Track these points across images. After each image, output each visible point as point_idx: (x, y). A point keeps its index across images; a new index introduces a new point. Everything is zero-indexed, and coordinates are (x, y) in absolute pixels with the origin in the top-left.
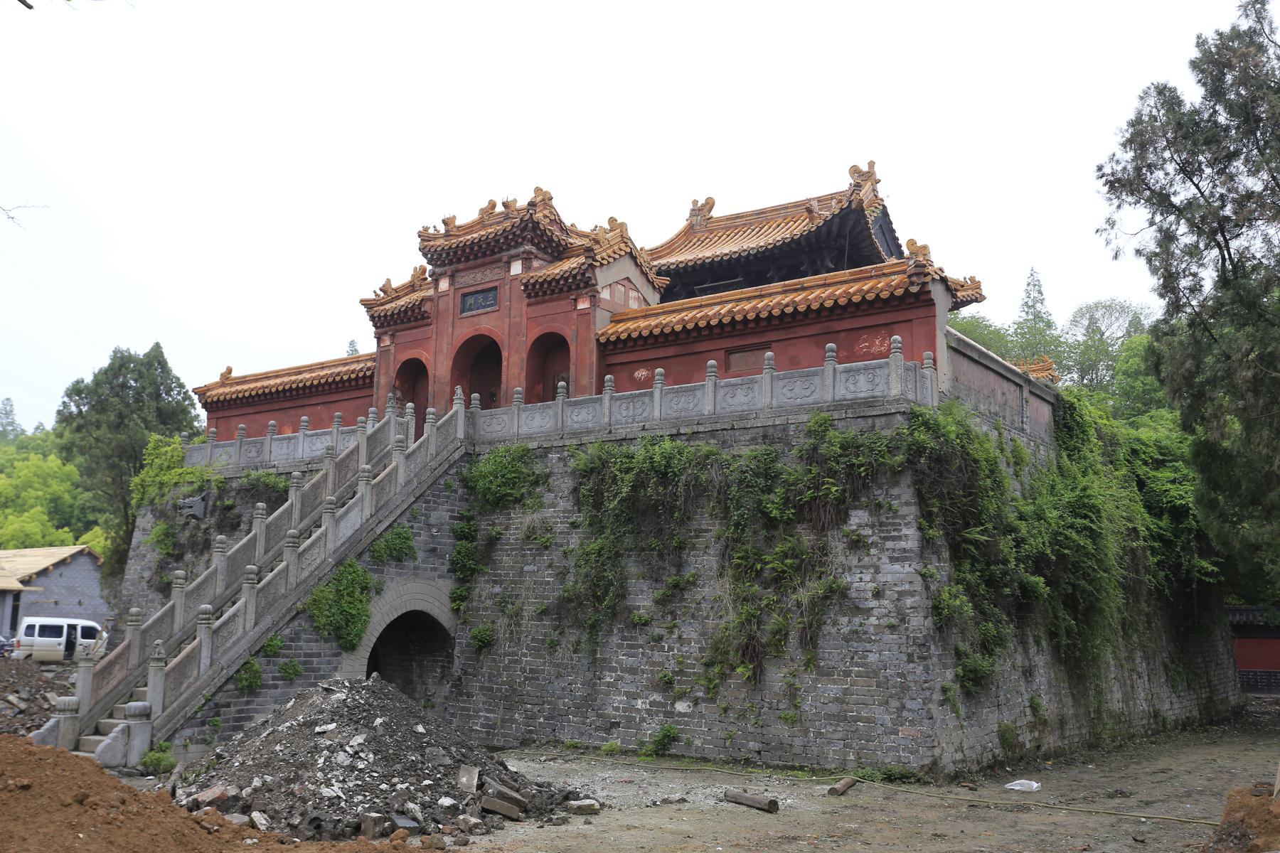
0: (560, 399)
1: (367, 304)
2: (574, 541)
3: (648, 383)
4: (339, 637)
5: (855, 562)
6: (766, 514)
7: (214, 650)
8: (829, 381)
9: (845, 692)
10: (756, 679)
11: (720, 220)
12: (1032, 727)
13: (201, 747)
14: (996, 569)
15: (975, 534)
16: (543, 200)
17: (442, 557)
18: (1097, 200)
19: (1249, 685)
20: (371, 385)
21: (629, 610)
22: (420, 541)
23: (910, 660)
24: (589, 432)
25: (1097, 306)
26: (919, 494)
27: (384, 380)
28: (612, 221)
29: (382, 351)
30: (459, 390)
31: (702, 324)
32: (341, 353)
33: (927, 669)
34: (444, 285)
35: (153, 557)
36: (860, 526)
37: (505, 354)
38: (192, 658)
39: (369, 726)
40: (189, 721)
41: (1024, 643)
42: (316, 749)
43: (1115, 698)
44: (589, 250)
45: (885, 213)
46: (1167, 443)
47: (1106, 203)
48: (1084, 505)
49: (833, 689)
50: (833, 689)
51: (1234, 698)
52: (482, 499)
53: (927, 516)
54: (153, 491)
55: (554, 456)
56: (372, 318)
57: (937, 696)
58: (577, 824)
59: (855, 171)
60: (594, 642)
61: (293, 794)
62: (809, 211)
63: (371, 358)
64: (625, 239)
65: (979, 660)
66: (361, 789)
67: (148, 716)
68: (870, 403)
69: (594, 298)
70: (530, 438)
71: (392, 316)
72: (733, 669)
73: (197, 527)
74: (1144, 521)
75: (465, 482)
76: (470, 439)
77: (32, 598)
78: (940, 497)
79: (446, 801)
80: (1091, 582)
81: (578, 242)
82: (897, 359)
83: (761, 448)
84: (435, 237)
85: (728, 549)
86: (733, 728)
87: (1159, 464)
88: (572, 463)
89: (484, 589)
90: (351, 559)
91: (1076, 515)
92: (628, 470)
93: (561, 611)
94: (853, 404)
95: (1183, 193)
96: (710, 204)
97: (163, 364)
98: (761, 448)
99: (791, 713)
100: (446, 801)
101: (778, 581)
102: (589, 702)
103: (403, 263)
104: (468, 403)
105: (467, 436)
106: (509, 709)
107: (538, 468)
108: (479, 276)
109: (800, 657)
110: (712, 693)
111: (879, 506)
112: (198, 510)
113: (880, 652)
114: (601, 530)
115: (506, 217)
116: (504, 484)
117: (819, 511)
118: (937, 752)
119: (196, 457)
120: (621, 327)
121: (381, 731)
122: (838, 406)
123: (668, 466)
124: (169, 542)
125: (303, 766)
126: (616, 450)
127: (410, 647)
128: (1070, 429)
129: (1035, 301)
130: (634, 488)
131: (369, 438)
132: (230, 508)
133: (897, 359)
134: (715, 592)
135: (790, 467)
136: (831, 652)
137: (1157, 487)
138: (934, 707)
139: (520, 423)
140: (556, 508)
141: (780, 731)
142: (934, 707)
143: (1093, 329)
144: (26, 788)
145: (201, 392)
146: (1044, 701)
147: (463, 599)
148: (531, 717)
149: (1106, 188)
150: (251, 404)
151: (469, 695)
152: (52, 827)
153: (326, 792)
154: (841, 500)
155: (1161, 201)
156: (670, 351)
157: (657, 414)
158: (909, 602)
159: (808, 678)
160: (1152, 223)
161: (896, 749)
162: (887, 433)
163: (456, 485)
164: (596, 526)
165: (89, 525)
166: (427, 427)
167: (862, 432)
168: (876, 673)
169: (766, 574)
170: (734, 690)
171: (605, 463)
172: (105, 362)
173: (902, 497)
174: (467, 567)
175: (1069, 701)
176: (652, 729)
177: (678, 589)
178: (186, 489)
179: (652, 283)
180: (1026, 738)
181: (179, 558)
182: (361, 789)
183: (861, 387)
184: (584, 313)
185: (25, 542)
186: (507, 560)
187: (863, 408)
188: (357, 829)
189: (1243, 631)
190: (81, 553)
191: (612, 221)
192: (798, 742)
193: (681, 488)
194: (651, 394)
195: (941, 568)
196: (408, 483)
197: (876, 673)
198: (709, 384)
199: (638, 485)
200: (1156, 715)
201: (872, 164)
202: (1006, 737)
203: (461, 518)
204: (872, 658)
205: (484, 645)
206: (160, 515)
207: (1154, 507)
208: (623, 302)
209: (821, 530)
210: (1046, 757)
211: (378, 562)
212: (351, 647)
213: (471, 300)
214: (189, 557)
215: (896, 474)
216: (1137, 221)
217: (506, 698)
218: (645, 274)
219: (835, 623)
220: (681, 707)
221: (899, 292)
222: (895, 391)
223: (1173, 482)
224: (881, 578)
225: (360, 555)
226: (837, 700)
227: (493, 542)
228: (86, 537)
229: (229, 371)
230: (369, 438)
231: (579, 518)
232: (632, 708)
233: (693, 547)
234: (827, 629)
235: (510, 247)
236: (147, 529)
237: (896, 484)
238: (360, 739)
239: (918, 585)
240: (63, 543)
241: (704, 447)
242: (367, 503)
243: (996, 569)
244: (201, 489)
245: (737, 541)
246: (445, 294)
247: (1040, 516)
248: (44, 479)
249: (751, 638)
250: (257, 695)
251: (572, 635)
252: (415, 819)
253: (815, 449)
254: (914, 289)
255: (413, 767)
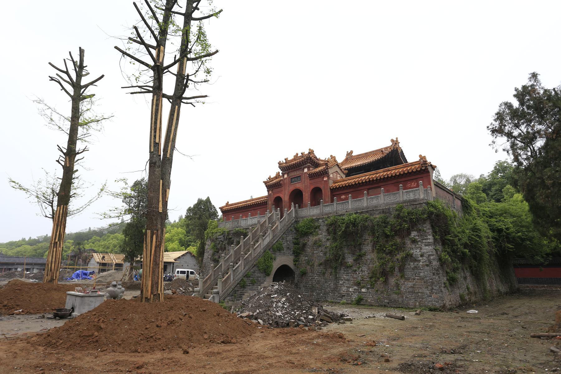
0: (321, 205)
1: (265, 183)
2: (328, 244)
3: (346, 199)
4: (265, 272)
5: (414, 246)
6: (386, 234)
7: (234, 276)
8: (401, 195)
9: (414, 285)
10: (386, 282)
11: (355, 156)
12: (468, 294)
13: (232, 302)
14: (455, 247)
15: (448, 237)
16: (311, 152)
17: (291, 249)
18: (490, 137)
19: (520, 282)
20: (267, 204)
21: (346, 263)
22: (285, 245)
23: (434, 274)
24: (331, 213)
25: (457, 176)
26: (432, 226)
27: (270, 202)
28: (331, 156)
29: (269, 195)
30: (293, 204)
31: (360, 182)
32: (249, 198)
33: (439, 277)
34: (286, 176)
35: (211, 252)
36: (414, 236)
37: (304, 194)
38: (229, 278)
39: (286, 295)
40: (229, 295)
41: (463, 269)
42: (272, 302)
43: (488, 287)
44: (327, 164)
45: (402, 152)
46: (493, 211)
47: (491, 136)
48: (476, 229)
49: (410, 284)
50: (410, 284)
51: (517, 286)
52: (301, 233)
53: (435, 232)
54: (210, 235)
55: (321, 221)
56: (266, 186)
57: (443, 285)
58: (348, 324)
59: (392, 141)
60: (336, 272)
61: (268, 314)
62: (382, 151)
63: (266, 197)
64: (335, 161)
65: (452, 274)
66: (287, 313)
67: (218, 293)
68: (415, 200)
69: (328, 177)
70: (313, 216)
71: (271, 185)
72: (379, 279)
73: (222, 244)
74: (491, 234)
75: (295, 229)
76: (296, 217)
77: (177, 264)
78: (439, 226)
79: (311, 317)
80: (480, 251)
81: (322, 162)
82: (421, 187)
83: (382, 215)
84: (282, 164)
85: (374, 244)
86: (380, 296)
87: (491, 217)
88: (326, 222)
89: (303, 258)
90: (267, 250)
91: (474, 232)
92: (343, 223)
93: (326, 264)
94: (410, 201)
95: (516, 133)
96: (352, 152)
97: (210, 202)
98: (382, 215)
99: (397, 291)
100: (311, 317)
101: (391, 253)
102: (336, 289)
103: (274, 171)
104: (295, 207)
105: (295, 216)
106: (312, 292)
107: (316, 224)
108: (295, 173)
109: (399, 275)
110: (372, 286)
111: (420, 230)
112: (222, 239)
113: (424, 273)
114: (336, 241)
115: (302, 157)
116: (307, 229)
117: (402, 232)
118: (445, 302)
119: (221, 225)
120: (337, 184)
121: (289, 297)
122: (405, 202)
123: (355, 221)
124: (215, 248)
125: (269, 306)
126: (339, 218)
127: (284, 273)
128: (467, 207)
129: (438, 175)
130: (346, 228)
131: (269, 218)
132: (231, 238)
133: (421, 187)
134: (371, 257)
135: (392, 220)
136: (408, 273)
137: (492, 223)
138: (442, 288)
139: (310, 212)
140: (322, 235)
141: (395, 296)
142: (442, 288)
143: (455, 182)
144: (205, 311)
145: (221, 208)
146: (470, 286)
147: (297, 261)
148: (318, 294)
149: (491, 133)
150: (233, 211)
151: (300, 288)
152: (212, 322)
153: (277, 314)
154: (408, 229)
155: (509, 135)
156: (351, 190)
157: (350, 207)
158: (432, 257)
159: (402, 281)
160: (508, 141)
161: (432, 301)
162: (421, 209)
163: (293, 230)
164: (335, 239)
165: (189, 246)
166: (285, 215)
167: (413, 209)
168: (423, 279)
169: (387, 251)
170: (379, 285)
171: (336, 222)
172: (196, 202)
173: (427, 227)
174: (297, 254)
175: (476, 286)
176: (355, 297)
177: (360, 256)
178: (219, 234)
179: (343, 172)
180: (467, 297)
181: (218, 252)
182: (287, 313)
183: (411, 196)
184: (326, 181)
185: (174, 250)
186: (309, 250)
187: (412, 202)
188: (288, 325)
189: (515, 266)
190: (188, 253)
191: (331, 156)
192: (400, 300)
193: (359, 227)
194: (348, 202)
195: (439, 247)
196: (281, 229)
197: (423, 279)
198: (365, 198)
199: (347, 227)
200: (499, 291)
201: (397, 138)
202: (462, 297)
203: (295, 239)
204: (422, 274)
205: (304, 274)
206: (213, 241)
207: (492, 230)
208: (336, 177)
209: (403, 238)
210: (473, 303)
211: (274, 251)
212: (268, 275)
213: (293, 180)
214: (220, 252)
215: (424, 220)
216: (503, 141)
217: (311, 289)
218: (341, 170)
219: (409, 265)
220: (363, 290)
221: (419, 169)
222: (422, 197)
223: (497, 222)
224: (422, 251)
225: (269, 249)
226: (411, 287)
227: (305, 245)
228: (188, 249)
229: (228, 202)
230: (269, 218)
231: (329, 237)
232: (349, 291)
233: (364, 244)
234: (406, 266)
235: (304, 165)
236: (209, 245)
237: (425, 223)
238: (284, 299)
239: (434, 253)
240: (183, 250)
241: (366, 216)
242: (271, 235)
243: (455, 247)
244: (223, 234)
245: (378, 242)
246: (286, 178)
247: (464, 232)
248: (178, 234)
249: (384, 270)
250: (245, 288)
251: (329, 270)
252: (303, 322)
253: (399, 214)
254: (423, 168)
255: (299, 307)
